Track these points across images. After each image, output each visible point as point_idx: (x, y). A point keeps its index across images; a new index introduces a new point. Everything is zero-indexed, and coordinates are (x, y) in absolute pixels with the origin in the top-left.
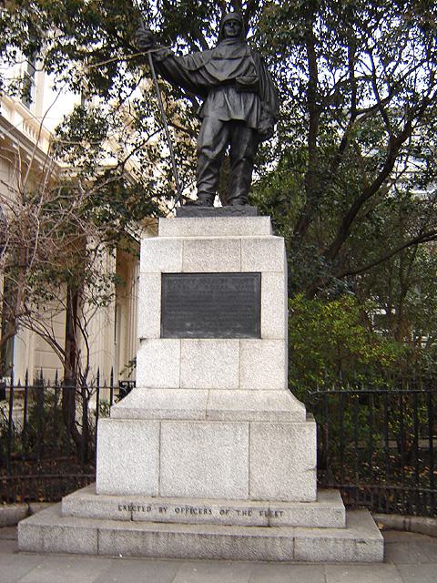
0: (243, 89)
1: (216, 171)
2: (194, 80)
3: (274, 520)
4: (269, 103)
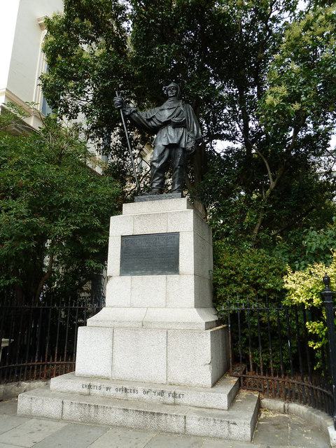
0: (176, 126)
1: (161, 175)
2: (150, 124)
3: (178, 400)
4: (193, 132)
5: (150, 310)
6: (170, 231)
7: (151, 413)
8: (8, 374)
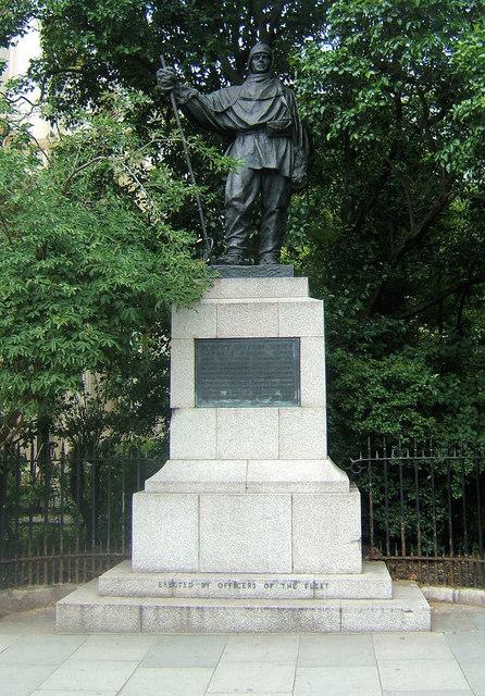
2: (221, 123)
3: (319, 592)
5: (256, 463)
6: (283, 334)
7: (290, 609)
8: (65, 573)
